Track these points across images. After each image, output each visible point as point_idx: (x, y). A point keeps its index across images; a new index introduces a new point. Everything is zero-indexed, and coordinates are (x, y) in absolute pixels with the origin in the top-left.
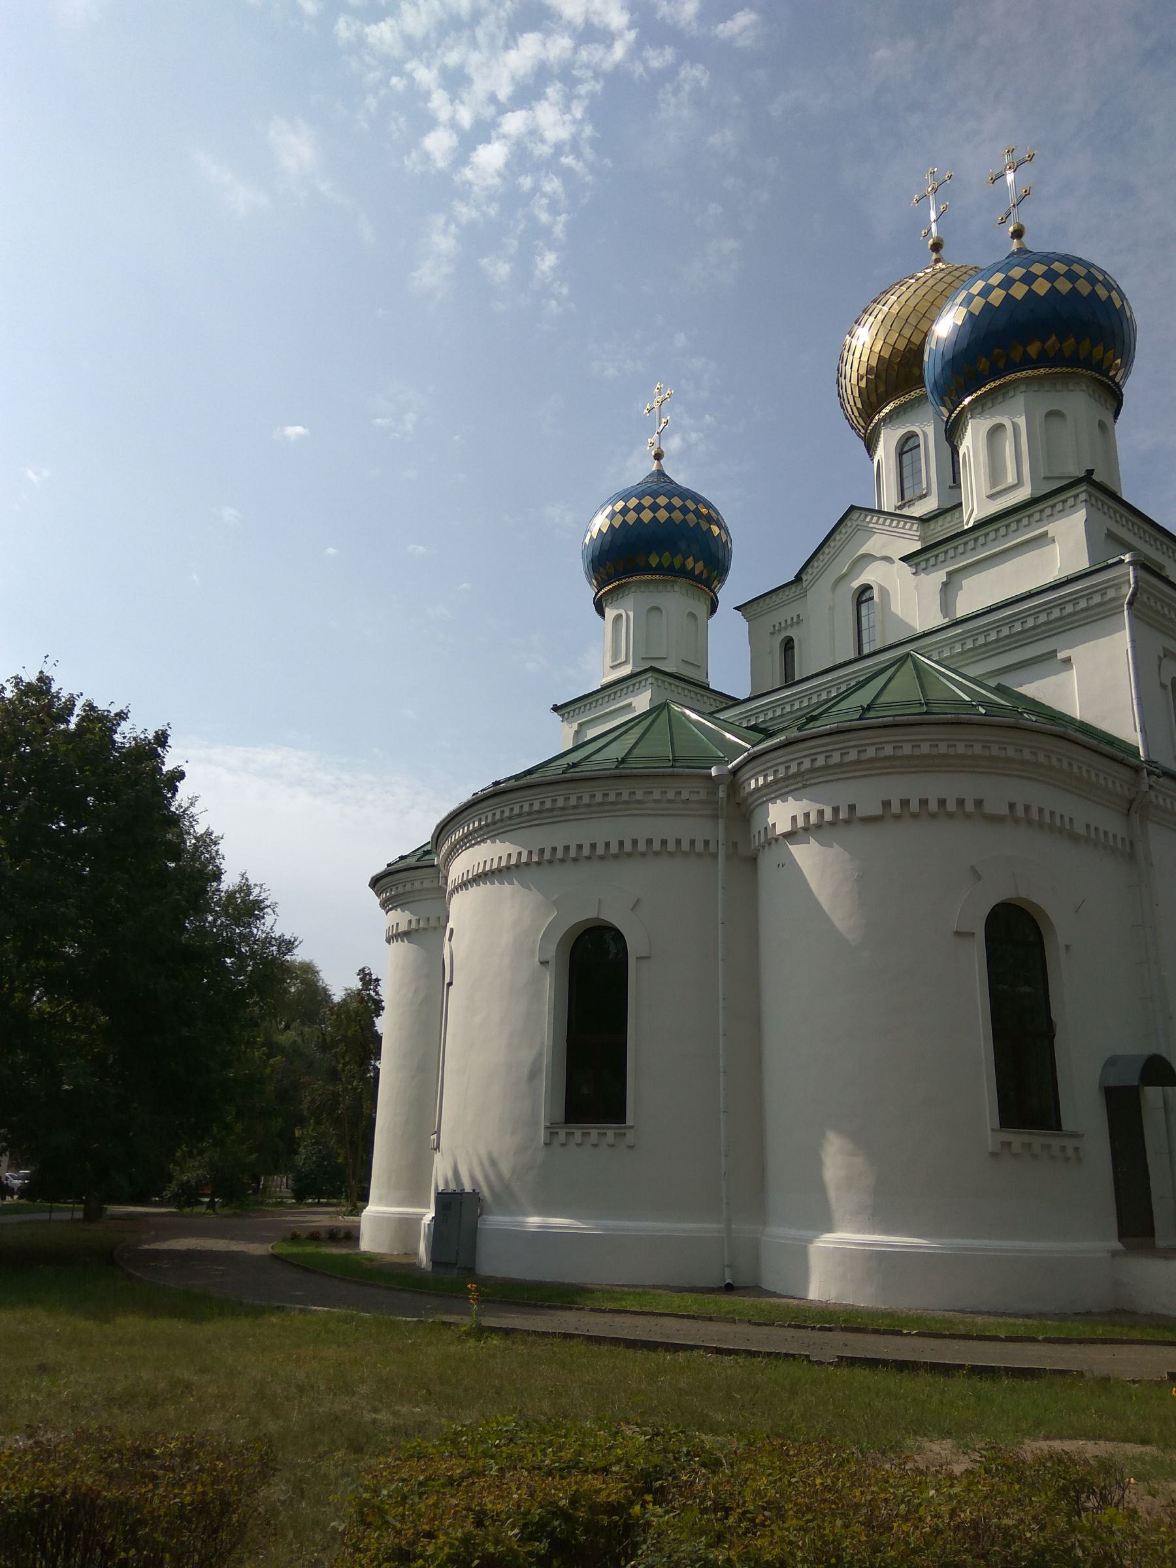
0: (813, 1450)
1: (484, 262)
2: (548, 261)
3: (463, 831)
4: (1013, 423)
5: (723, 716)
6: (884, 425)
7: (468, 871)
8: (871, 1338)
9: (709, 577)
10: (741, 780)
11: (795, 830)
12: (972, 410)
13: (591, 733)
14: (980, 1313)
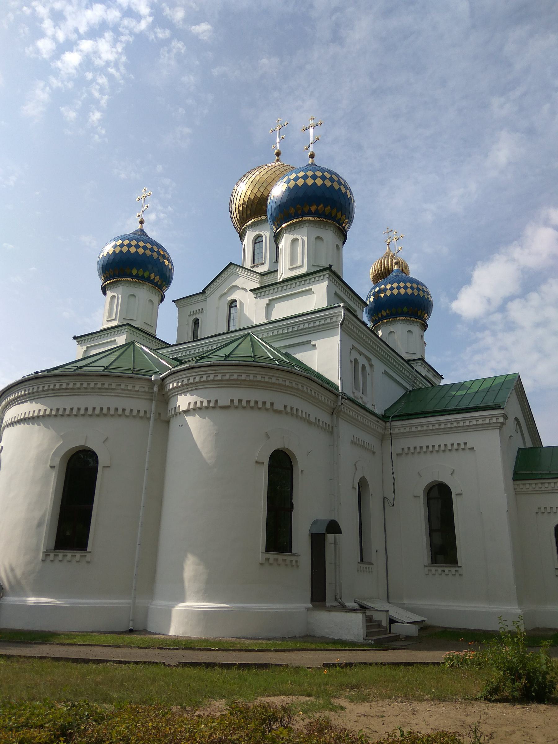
0: (151, 709)
1: (62, 109)
2: (96, 116)
3: (15, 395)
4: (302, 239)
5: (161, 351)
6: (248, 229)
7: (15, 417)
8: (196, 652)
9: (161, 284)
10: (166, 383)
11: (195, 408)
12: (285, 230)
13: (93, 352)
14: (247, 638)
